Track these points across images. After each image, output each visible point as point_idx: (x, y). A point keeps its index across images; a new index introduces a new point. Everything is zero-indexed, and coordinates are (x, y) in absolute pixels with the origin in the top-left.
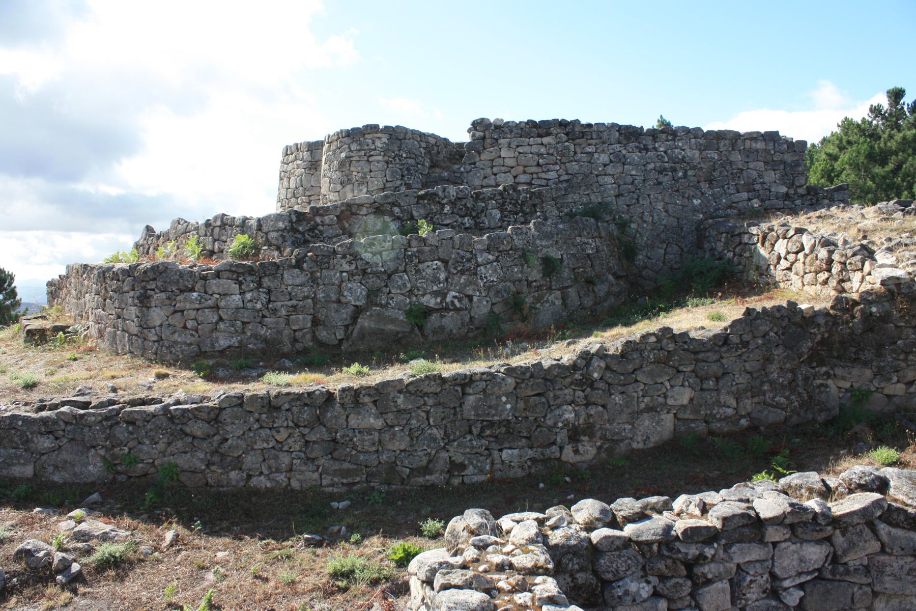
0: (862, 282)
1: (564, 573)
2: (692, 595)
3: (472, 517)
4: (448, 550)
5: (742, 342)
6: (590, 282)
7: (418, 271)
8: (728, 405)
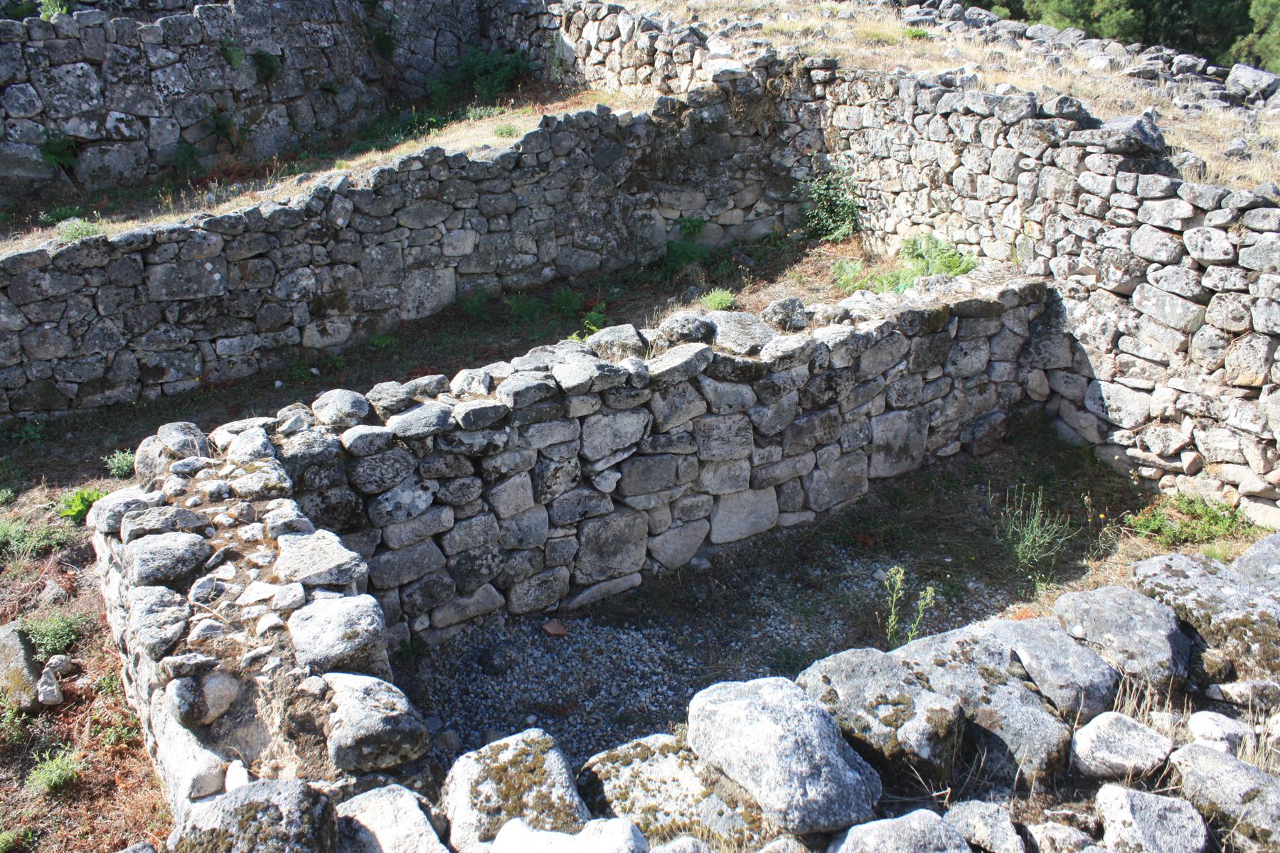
0: (691, 78)
1: (311, 492)
2: (484, 497)
3: (170, 435)
4: (143, 487)
5: (539, 164)
6: (327, 90)
7: (51, 80)
8: (526, 251)
